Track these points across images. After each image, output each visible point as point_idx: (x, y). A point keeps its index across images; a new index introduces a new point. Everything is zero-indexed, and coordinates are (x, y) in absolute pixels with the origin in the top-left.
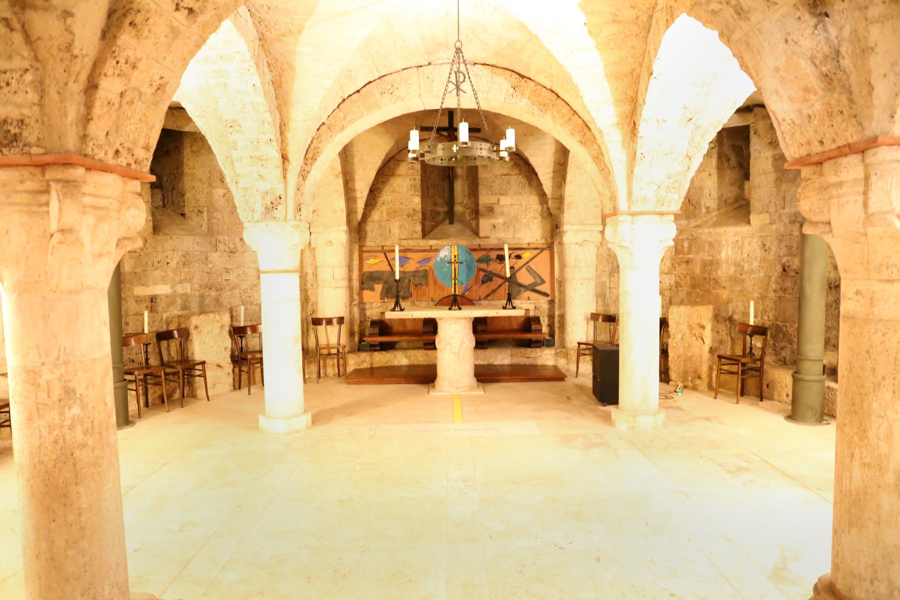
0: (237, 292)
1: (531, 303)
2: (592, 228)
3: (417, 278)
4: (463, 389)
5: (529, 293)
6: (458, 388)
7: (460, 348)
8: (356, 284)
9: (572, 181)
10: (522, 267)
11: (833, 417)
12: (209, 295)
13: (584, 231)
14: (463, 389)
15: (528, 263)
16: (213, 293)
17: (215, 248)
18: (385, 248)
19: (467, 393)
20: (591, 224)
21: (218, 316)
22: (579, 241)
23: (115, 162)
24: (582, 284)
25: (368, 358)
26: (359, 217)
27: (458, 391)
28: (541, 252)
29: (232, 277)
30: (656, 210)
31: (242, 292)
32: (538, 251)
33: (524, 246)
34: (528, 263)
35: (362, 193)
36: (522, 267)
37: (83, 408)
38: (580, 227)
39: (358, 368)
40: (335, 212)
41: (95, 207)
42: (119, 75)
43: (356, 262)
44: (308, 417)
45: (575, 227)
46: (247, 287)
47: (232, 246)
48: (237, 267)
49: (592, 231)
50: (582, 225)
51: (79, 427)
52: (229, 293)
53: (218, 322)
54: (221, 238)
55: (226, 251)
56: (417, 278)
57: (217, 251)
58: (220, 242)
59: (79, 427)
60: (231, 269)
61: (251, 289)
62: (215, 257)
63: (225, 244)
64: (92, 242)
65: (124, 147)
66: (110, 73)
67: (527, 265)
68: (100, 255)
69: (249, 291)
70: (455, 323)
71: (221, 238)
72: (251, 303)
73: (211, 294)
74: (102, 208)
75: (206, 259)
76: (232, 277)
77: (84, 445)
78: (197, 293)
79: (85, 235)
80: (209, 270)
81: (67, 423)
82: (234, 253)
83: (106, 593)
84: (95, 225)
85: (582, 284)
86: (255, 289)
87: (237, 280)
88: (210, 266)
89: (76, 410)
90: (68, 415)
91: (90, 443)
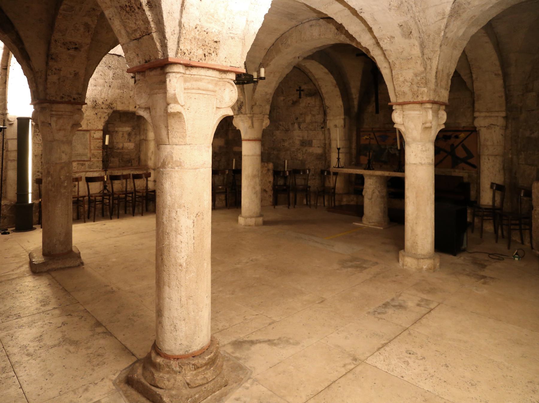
0: (288, 152)
1: (466, 172)
2: (496, 114)
3: (393, 150)
4: (373, 224)
5: (462, 165)
6: (370, 223)
7: (372, 195)
8: (354, 151)
9: (477, 78)
10: (459, 145)
11: (425, 270)
12: (273, 153)
13: (490, 117)
14: (373, 224)
15: (463, 141)
16: (275, 152)
17: (278, 129)
18: (374, 130)
19: (379, 228)
20: (497, 111)
21: (266, 164)
22: (486, 125)
23: (61, 100)
24: (489, 159)
25: (355, 199)
26: (356, 109)
27: (368, 224)
28: (470, 134)
29: (286, 144)
30: (414, 101)
31: (291, 152)
32: (469, 133)
33: (460, 129)
34: (463, 141)
35: (355, 95)
36: (459, 145)
37: (52, 178)
38: (487, 114)
39: (349, 204)
40: (338, 107)
41: (56, 115)
42: (54, 74)
43: (354, 138)
44: (260, 220)
45: (483, 114)
46: (294, 150)
47: (287, 127)
48: (289, 139)
49: (497, 116)
50: (488, 112)
51: (50, 184)
52: (284, 153)
53: (266, 167)
54: (281, 123)
55: (283, 130)
56: (393, 150)
57: (278, 130)
58: (280, 125)
59: (50, 184)
60: (286, 140)
61: (296, 151)
62: (278, 133)
63: (283, 126)
64: (56, 126)
65: (65, 95)
66: (50, 74)
67: (462, 144)
68: (60, 130)
69: (296, 153)
70: (370, 179)
71: (281, 123)
72: (296, 159)
73: (275, 153)
74: (60, 115)
75: (273, 134)
76: (286, 144)
77: (51, 190)
78: (267, 152)
79: (53, 124)
80: (273, 140)
81: (48, 182)
82: (288, 131)
83: (55, 241)
84: (56, 121)
85: (489, 159)
86: (299, 151)
87: (289, 146)
88: (274, 138)
89: (50, 179)
90: (48, 180)
91: (53, 190)
